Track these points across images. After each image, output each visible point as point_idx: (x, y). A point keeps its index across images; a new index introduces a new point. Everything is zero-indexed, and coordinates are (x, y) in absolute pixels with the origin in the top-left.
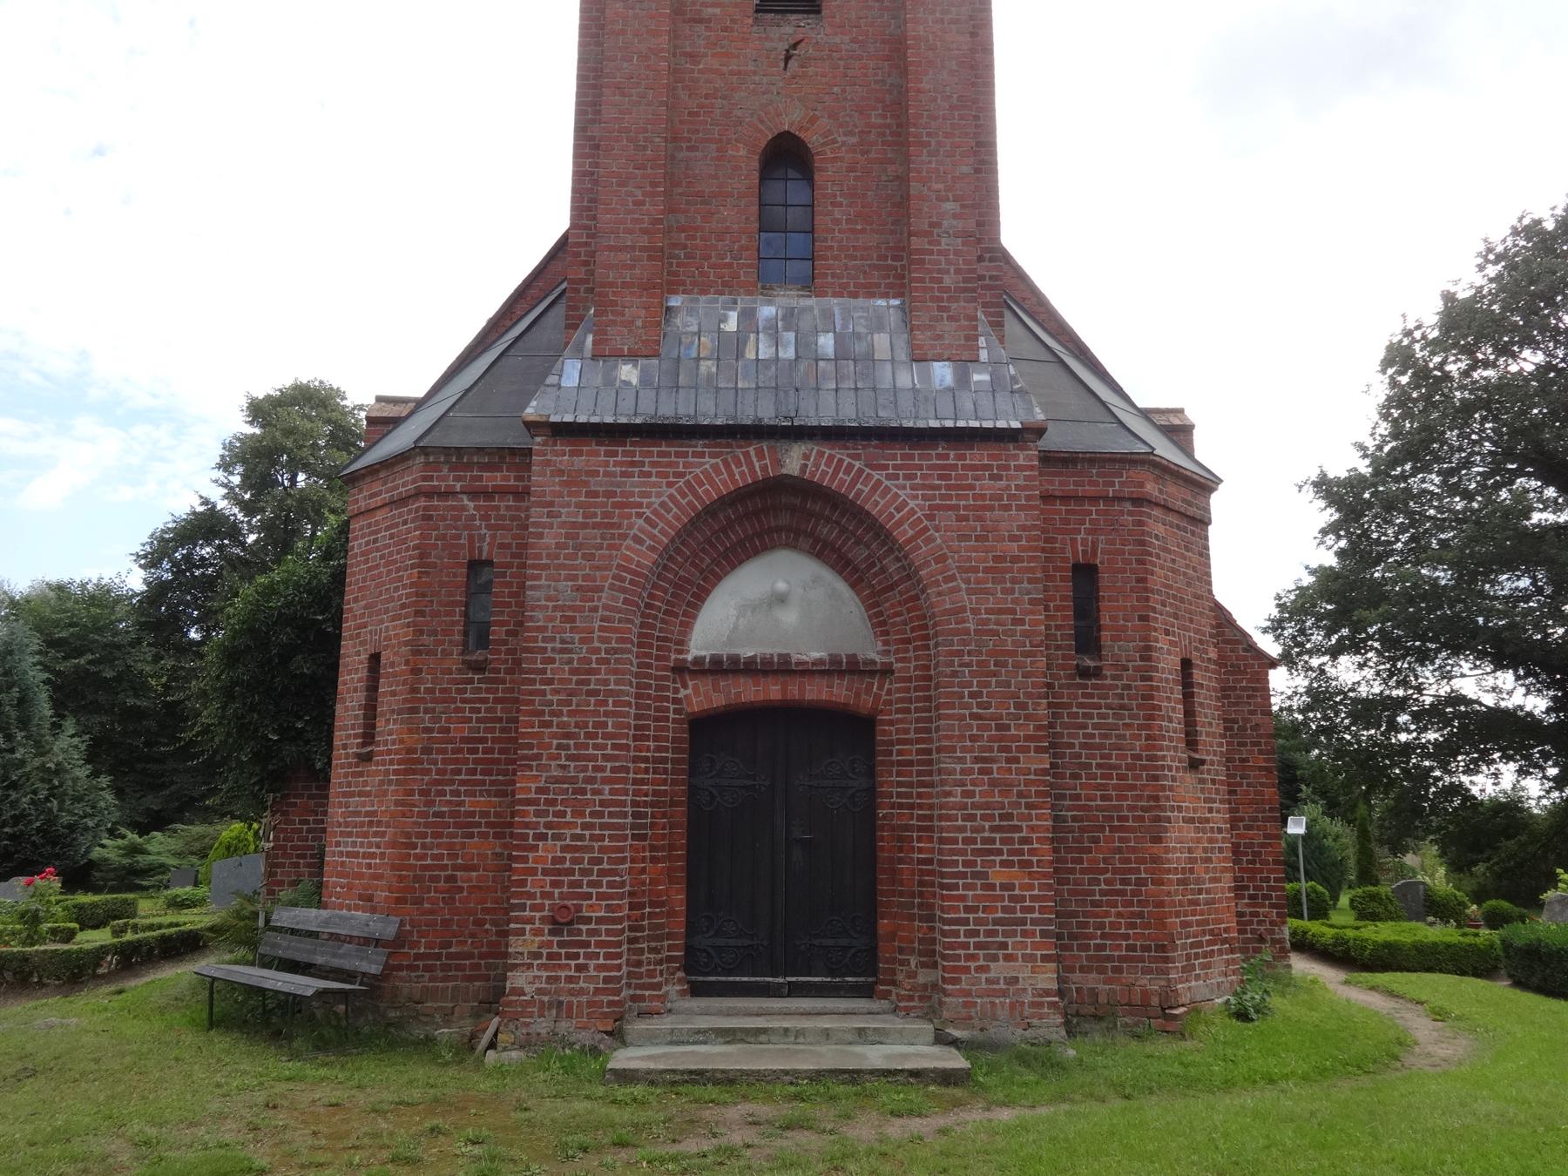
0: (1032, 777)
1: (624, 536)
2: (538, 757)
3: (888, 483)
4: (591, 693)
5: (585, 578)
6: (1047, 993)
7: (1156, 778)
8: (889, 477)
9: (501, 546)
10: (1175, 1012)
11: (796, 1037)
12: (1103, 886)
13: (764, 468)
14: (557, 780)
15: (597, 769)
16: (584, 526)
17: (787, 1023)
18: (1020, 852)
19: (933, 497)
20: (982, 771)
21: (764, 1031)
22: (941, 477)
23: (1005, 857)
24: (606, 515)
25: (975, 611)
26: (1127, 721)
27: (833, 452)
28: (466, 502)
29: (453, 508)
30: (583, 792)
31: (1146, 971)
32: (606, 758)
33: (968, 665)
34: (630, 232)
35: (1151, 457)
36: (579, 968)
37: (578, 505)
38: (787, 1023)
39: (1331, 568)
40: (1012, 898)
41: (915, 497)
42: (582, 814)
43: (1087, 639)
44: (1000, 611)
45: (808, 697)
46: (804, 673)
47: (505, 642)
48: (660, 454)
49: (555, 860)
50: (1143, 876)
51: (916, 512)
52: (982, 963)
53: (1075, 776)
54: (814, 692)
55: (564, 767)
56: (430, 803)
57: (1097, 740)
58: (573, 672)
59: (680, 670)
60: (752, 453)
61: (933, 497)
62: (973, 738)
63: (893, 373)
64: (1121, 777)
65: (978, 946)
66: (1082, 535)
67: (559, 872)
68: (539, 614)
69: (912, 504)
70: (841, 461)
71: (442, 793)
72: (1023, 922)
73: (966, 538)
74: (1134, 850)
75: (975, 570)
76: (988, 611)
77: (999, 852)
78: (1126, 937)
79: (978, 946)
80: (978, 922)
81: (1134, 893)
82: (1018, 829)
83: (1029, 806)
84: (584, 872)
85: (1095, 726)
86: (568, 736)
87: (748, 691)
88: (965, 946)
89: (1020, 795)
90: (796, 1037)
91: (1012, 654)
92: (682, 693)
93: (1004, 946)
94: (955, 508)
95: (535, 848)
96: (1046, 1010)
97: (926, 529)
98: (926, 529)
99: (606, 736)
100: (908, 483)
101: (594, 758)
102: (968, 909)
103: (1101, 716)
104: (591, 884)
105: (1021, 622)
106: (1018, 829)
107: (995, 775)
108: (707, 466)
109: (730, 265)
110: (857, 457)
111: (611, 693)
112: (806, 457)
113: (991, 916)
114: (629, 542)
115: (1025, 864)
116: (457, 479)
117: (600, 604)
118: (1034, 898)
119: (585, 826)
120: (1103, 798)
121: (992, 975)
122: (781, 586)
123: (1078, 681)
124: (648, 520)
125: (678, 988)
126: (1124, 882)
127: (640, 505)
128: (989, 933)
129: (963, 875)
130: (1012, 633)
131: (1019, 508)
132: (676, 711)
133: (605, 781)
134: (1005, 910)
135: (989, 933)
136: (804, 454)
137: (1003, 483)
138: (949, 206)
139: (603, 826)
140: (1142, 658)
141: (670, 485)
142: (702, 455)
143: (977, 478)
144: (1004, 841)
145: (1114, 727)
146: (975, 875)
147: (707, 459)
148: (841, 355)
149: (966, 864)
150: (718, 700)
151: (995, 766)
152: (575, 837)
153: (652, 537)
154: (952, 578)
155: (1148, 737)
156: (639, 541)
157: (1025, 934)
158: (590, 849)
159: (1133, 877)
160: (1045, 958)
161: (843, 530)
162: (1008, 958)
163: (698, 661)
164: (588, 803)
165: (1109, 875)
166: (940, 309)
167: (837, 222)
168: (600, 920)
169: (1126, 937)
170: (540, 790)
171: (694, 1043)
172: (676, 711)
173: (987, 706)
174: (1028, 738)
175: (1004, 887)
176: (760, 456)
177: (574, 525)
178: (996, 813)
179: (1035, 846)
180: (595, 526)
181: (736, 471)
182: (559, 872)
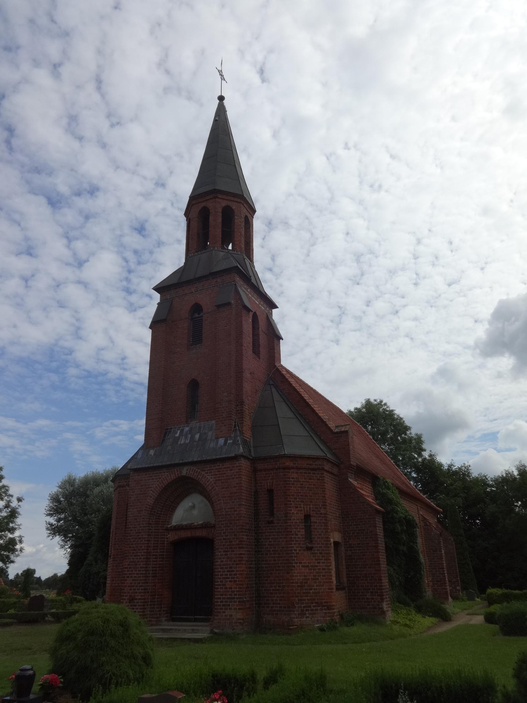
0: (238, 556)
3: (205, 475)
6: (240, 619)
8: (206, 473)
10: (291, 627)
11: (178, 631)
12: (273, 588)
13: (178, 474)
17: (176, 627)
18: (234, 578)
19: (216, 478)
20: (226, 555)
21: (171, 629)
22: (218, 472)
23: (230, 579)
25: (225, 509)
26: (281, 536)
27: (193, 468)
28: (127, 488)
33: (223, 524)
35: (285, 455)
38: (176, 627)
39: (16, 546)
40: (232, 592)
41: (212, 478)
42: (136, 571)
46: (196, 528)
48: (157, 473)
49: (131, 583)
50: (284, 584)
51: (212, 482)
52: (223, 610)
53: (266, 554)
54: (199, 533)
57: (272, 543)
59: (167, 529)
60: (176, 470)
61: (216, 478)
62: (224, 545)
63: (210, 443)
65: (223, 605)
66: (269, 481)
70: (195, 470)
71: (120, 566)
72: (234, 598)
73: (223, 488)
76: (228, 509)
77: (229, 578)
78: (279, 604)
79: (223, 605)
80: (223, 598)
82: (233, 571)
83: (237, 564)
85: (272, 539)
86: (135, 550)
87: (183, 534)
88: (220, 605)
89: (234, 561)
90: (178, 631)
92: (169, 536)
93: (229, 605)
96: (238, 624)
97: (214, 487)
98: (214, 487)
100: (210, 474)
101: (139, 556)
103: (274, 535)
104: (138, 590)
105: (236, 511)
106: (233, 571)
107: (229, 556)
108: (166, 475)
110: (198, 469)
112: (187, 470)
113: (226, 597)
114: (149, 497)
115: (235, 581)
117: (142, 515)
118: (237, 591)
120: (274, 560)
121: (226, 614)
122: (190, 504)
123: (268, 525)
124: (153, 492)
125: (165, 618)
126: (279, 586)
127: (151, 487)
129: (220, 585)
131: (237, 478)
132: (167, 541)
134: (230, 595)
136: (187, 469)
137: (233, 471)
138: (225, 394)
140: (285, 517)
141: (158, 481)
142: (165, 472)
143: (226, 471)
144: (230, 575)
147: (166, 473)
148: (200, 439)
149: (221, 582)
151: (228, 553)
152: (135, 577)
154: (220, 500)
155: (286, 541)
157: (234, 602)
159: (282, 585)
160: (239, 609)
162: (230, 609)
163: (175, 527)
165: (275, 584)
169: (279, 604)
171: (157, 632)
172: (167, 541)
173: (227, 536)
178: (228, 567)
179: (238, 576)
181: (172, 476)
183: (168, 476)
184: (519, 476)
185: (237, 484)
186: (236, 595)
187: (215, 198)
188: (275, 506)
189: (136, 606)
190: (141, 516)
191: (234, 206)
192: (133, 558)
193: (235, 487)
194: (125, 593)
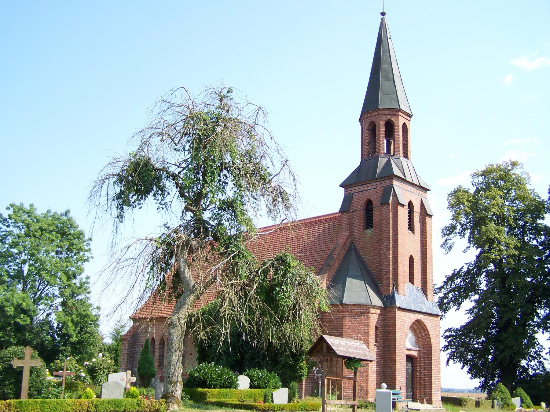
4: (402, 353)
56: (372, 369)
71: (373, 367)
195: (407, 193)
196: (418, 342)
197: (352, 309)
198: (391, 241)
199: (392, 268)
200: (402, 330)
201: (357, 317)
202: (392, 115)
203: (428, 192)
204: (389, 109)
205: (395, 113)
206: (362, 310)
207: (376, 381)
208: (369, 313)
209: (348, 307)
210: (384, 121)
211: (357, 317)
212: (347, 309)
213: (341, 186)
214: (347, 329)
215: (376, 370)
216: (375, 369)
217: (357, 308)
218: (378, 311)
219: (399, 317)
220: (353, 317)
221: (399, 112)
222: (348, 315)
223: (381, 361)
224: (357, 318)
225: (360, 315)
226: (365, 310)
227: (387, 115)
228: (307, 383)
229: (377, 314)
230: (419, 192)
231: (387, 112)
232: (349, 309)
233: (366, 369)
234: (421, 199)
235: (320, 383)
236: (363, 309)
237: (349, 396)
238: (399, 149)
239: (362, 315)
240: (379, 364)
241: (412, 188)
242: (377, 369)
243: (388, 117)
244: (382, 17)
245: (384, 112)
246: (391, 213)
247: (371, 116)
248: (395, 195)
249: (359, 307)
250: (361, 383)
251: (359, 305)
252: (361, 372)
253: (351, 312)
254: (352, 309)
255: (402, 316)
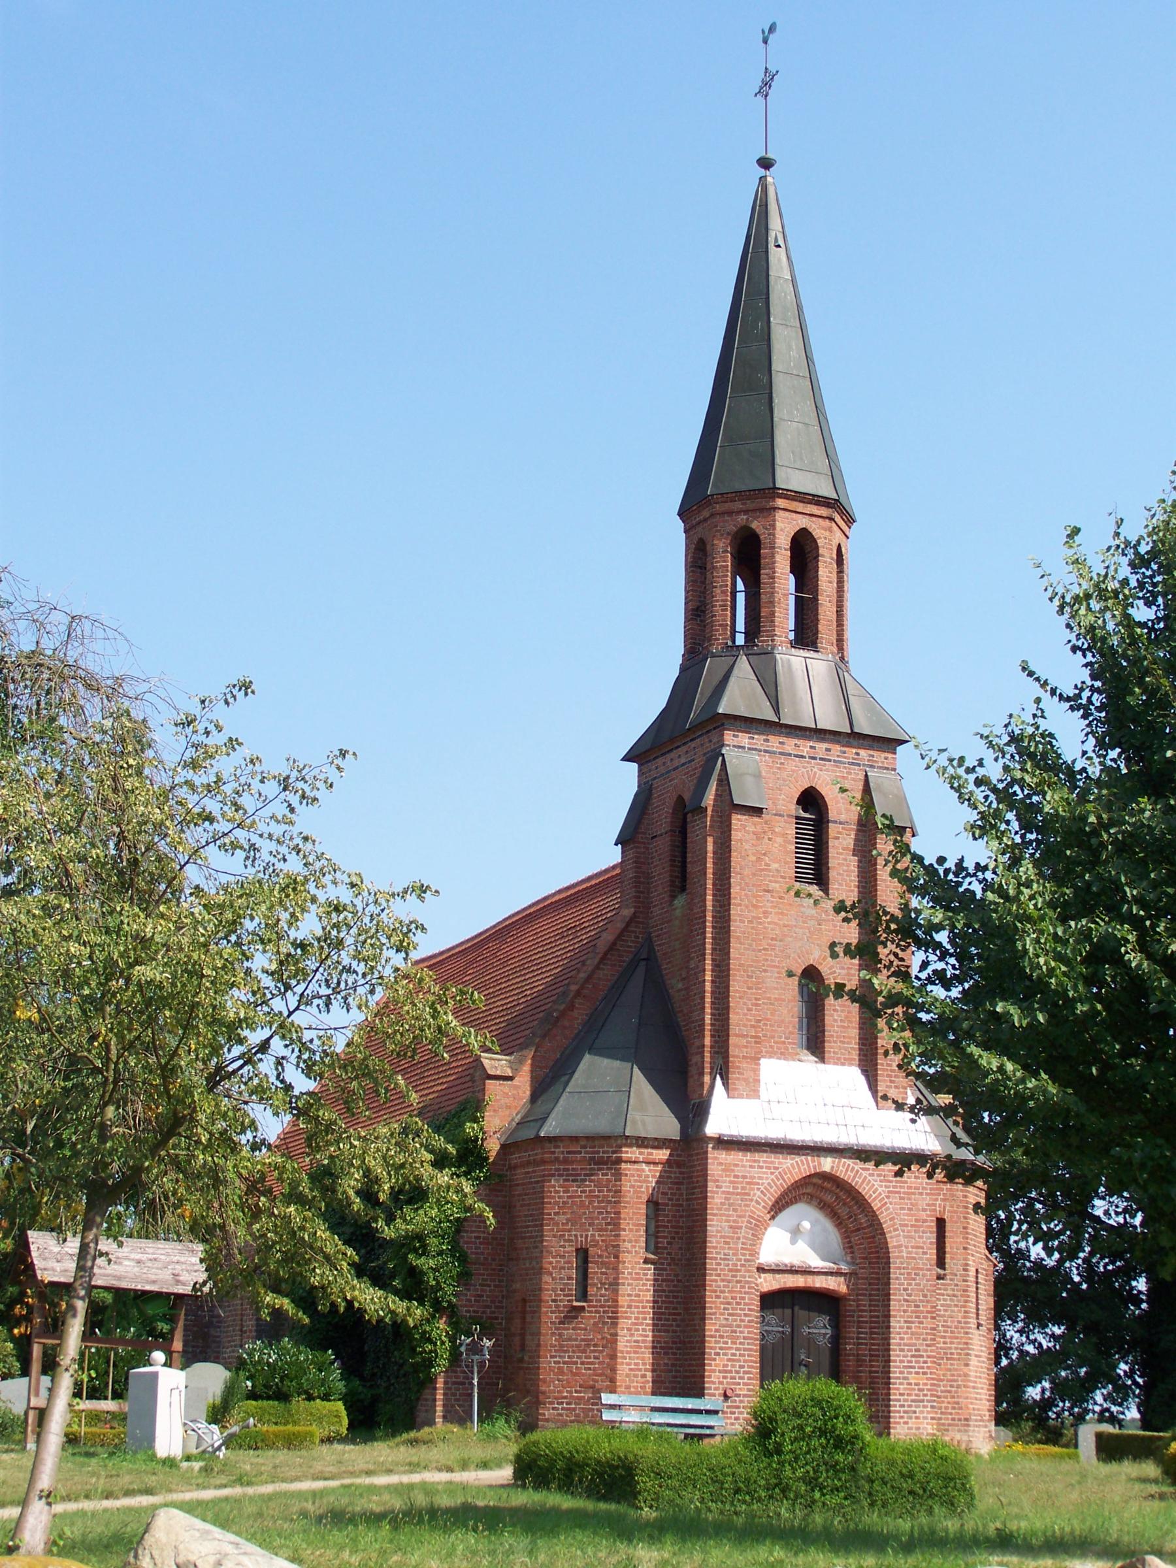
1: (752, 1200)
2: (715, 1314)
4: (738, 1282)
5: (734, 1221)
7: (967, 1333)
9: (663, 1193)
13: (815, 1167)
14: (724, 1326)
15: (741, 1321)
16: (733, 1193)
20: (908, 1328)
24: (743, 1188)
29: (638, 1170)
30: (735, 1332)
31: (959, 1431)
32: (745, 1315)
34: (745, 1026)
36: (736, 1419)
37: (731, 1182)
40: (920, 1390)
43: (941, 1262)
44: (918, 1247)
45: (818, 1285)
47: (666, 1248)
49: (725, 1366)
55: (727, 1319)
56: (632, 1335)
58: (730, 1270)
59: (761, 1269)
62: (905, 1311)
64: (952, 1332)
67: (726, 1372)
68: (714, 1240)
69: (880, 1190)
71: (638, 1330)
72: (923, 1401)
74: (956, 1370)
75: (906, 1225)
79: (905, 1412)
80: (905, 1400)
81: (956, 1392)
84: (737, 1372)
86: (728, 1303)
91: (922, 1269)
94: (899, 1193)
95: (715, 1360)
99: (745, 1304)
101: (740, 1315)
102: (901, 1394)
103: (945, 1300)
104: (740, 1378)
106: (922, 1356)
109: (784, 1043)
111: (747, 1282)
116: (641, 1153)
119: (737, 1349)
120: (945, 1343)
126: (952, 1386)
128: (909, 1406)
130: (921, 1259)
133: (746, 1327)
135: (909, 1406)
139: (745, 1350)
141: (772, 1173)
144: (916, 1362)
145: (950, 1306)
146: (905, 1378)
150: (775, 1286)
153: (765, 1201)
154: (896, 1230)
156: (758, 1203)
157: (924, 1406)
158: (739, 1361)
161: (837, 1198)
162: (917, 1418)
164: (738, 1337)
166: (891, 1082)
167: (836, 1021)
168: (745, 1396)
170: (717, 1331)
174: (928, 1312)
175: (916, 1384)
176: (813, 1161)
177: (728, 1193)
180: (738, 1194)
182: (726, 1372)
183: (796, 1167)
184: (457, 1151)
185: (928, 1205)
186: (925, 1395)
187: (832, 519)
188: (948, 1249)
189: (738, 1407)
190: (739, 1238)
191: (818, 529)
192: (727, 1319)
193: (924, 1210)
194: (714, 1383)
195: (792, 764)
196: (851, 1247)
197: (568, 1152)
198: (709, 930)
199: (712, 1014)
200: (734, 1210)
201: (586, 1175)
202: (754, 510)
203: (900, 749)
204: (740, 495)
205: (763, 503)
206: (598, 1152)
207: (649, 1374)
208: (619, 1161)
209: (558, 1147)
210: (728, 534)
211: (586, 1175)
212: (554, 1153)
213: (627, 758)
214: (556, 1214)
215: (650, 1339)
216: (647, 1336)
217: (584, 1147)
218: (663, 1154)
219: (723, 1170)
220: (572, 1175)
221: (773, 498)
222: (559, 1170)
223: (676, 1308)
224: (585, 1180)
225: (593, 1169)
226: (607, 1152)
227: (739, 512)
228: (454, 1383)
229: (655, 1163)
230: (857, 754)
231: (738, 505)
232: (560, 1151)
233: (611, 1335)
234: (866, 776)
235: (475, 1382)
236: (603, 1152)
237: (558, 1421)
238: (773, 621)
239: (599, 1169)
240: (668, 1320)
241: (817, 745)
242: (653, 1336)
243: (742, 518)
244: (762, 172)
245: (727, 505)
246: (710, 840)
247: (699, 523)
248: (724, 781)
249: (590, 1143)
250: (594, 1380)
251: (587, 1138)
252: (595, 1345)
253: (566, 1161)
254: (568, 1152)
255: (737, 1165)
